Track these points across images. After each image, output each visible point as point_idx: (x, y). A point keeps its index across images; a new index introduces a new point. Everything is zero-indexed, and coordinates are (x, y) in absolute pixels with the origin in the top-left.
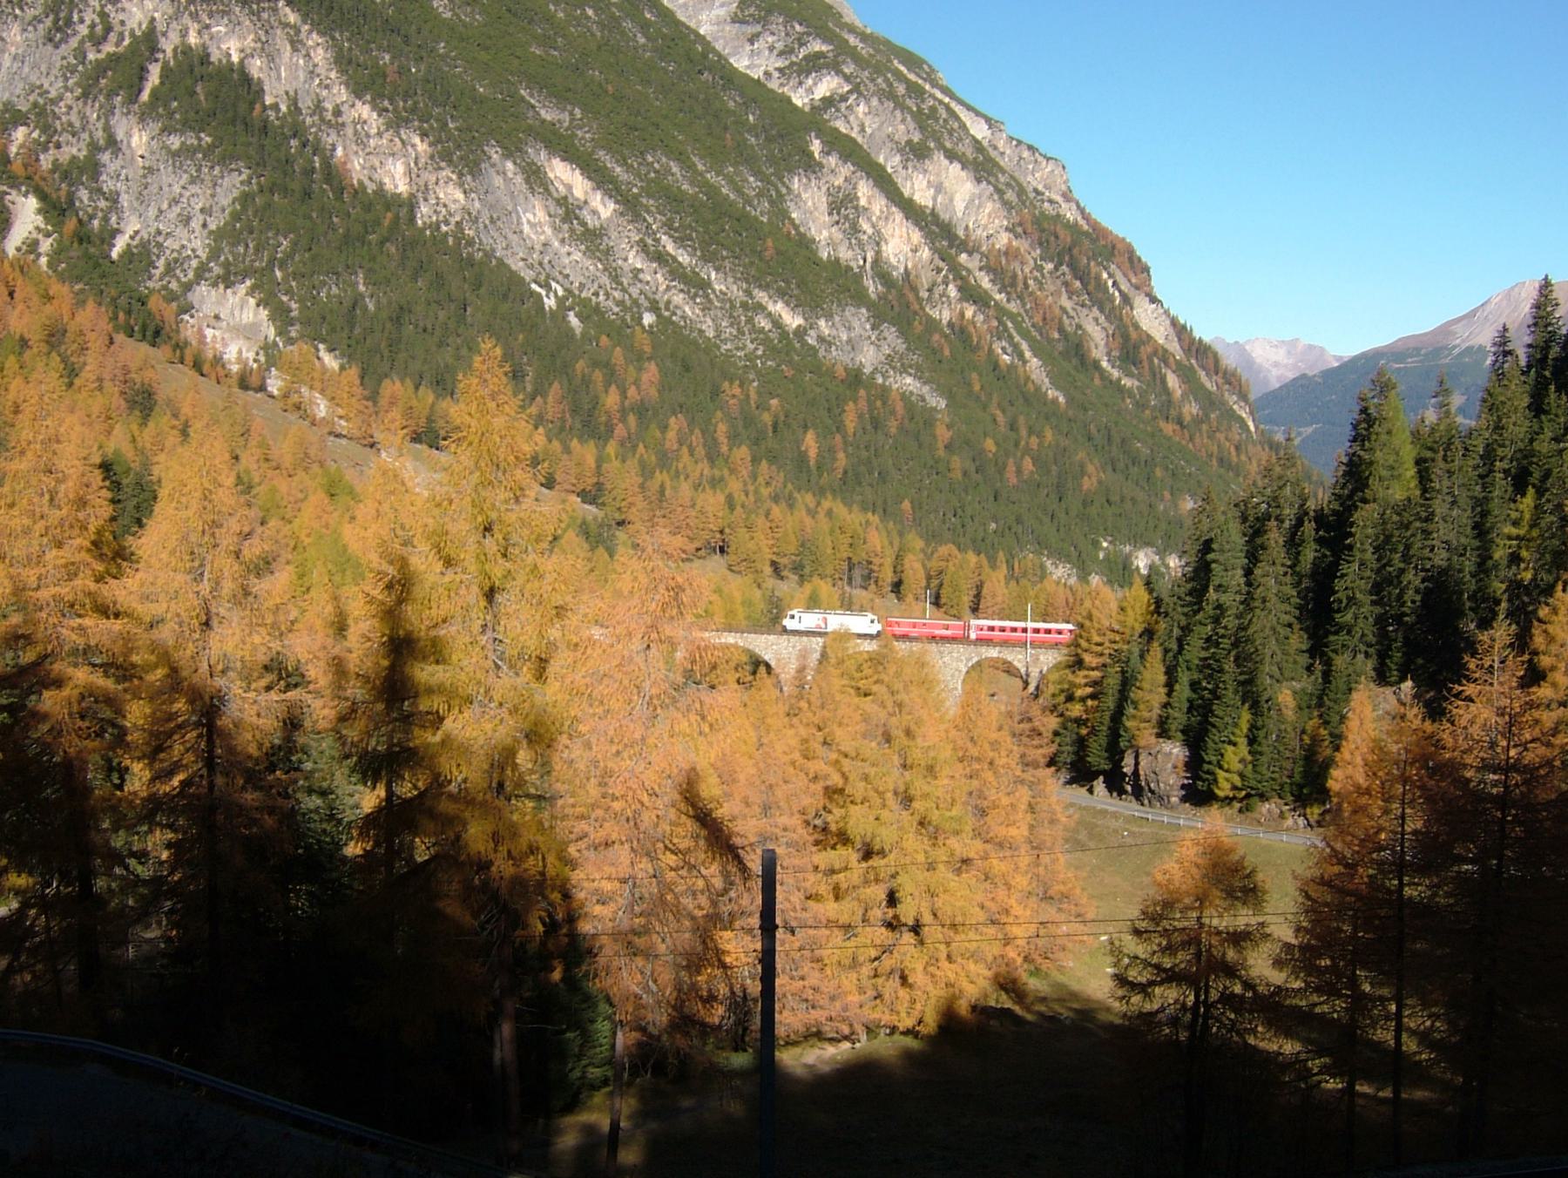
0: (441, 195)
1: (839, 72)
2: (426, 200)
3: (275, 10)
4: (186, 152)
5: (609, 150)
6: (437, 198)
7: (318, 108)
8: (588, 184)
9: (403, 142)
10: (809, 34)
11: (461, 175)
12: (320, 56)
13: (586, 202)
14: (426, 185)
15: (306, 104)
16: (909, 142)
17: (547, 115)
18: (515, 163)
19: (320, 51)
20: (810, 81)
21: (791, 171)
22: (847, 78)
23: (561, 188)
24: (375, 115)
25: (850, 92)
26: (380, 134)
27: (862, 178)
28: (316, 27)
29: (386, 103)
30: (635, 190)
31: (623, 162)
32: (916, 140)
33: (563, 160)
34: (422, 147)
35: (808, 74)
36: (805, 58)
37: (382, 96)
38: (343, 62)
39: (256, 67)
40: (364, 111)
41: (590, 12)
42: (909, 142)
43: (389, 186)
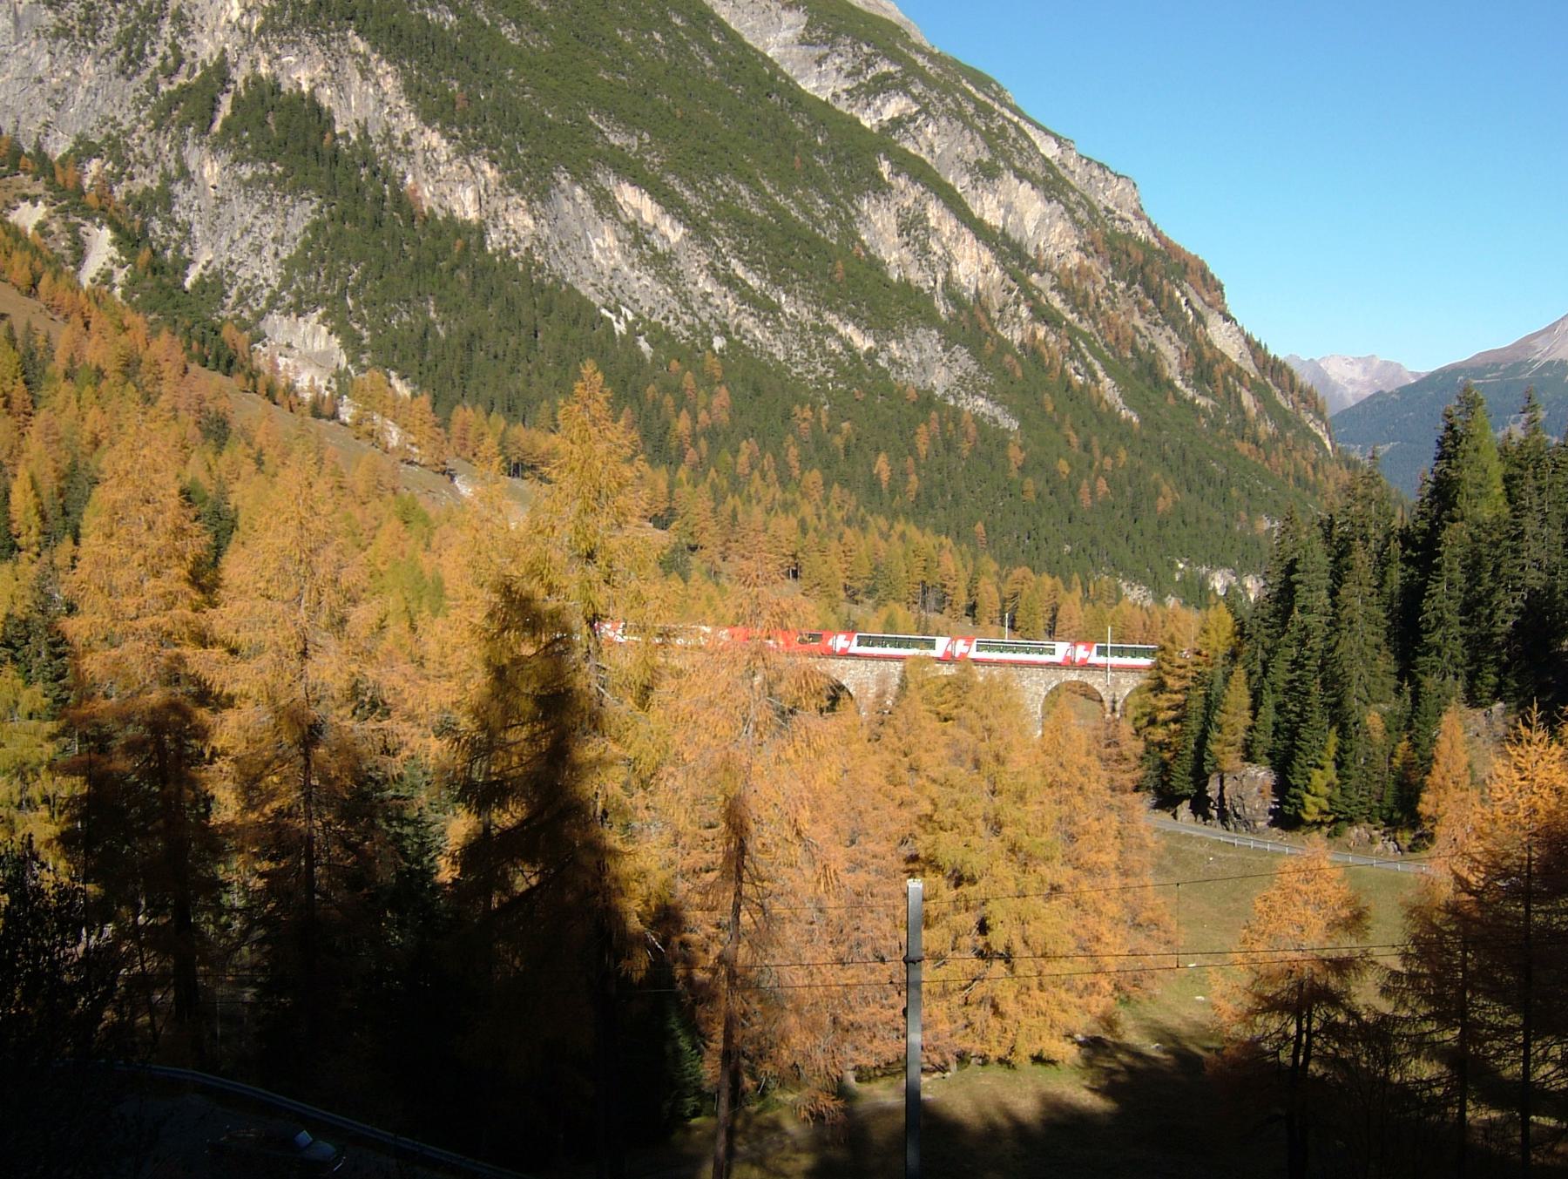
0: (511, 222)
1: (907, 93)
2: (496, 226)
3: (345, 39)
4: (258, 181)
5: (678, 174)
6: (507, 224)
7: (388, 136)
8: (657, 209)
9: (472, 169)
10: (876, 55)
11: (530, 201)
12: (389, 84)
13: (655, 227)
14: (496, 212)
15: (375, 132)
16: (978, 162)
17: (615, 140)
18: (584, 188)
19: (390, 79)
20: (878, 103)
21: (860, 193)
22: (915, 99)
23: (630, 213)
24: (444, 143)
25: (918, 112)
26: (449, 162)
27: (931, 199)
28: (386, 55)
29: (455, 131)
30: (704, 214)
31: (692, 186)
32: (985, 159)
33: (633, 184)
34: (491, 173)
35: (876, 94)
36: (873, 79)
37: (451, 123)
38: (412, 90)
39: (326, 96)
40: (434, 138)
41: (657, 36)
42: (978, 162)
43: (459, 213)
